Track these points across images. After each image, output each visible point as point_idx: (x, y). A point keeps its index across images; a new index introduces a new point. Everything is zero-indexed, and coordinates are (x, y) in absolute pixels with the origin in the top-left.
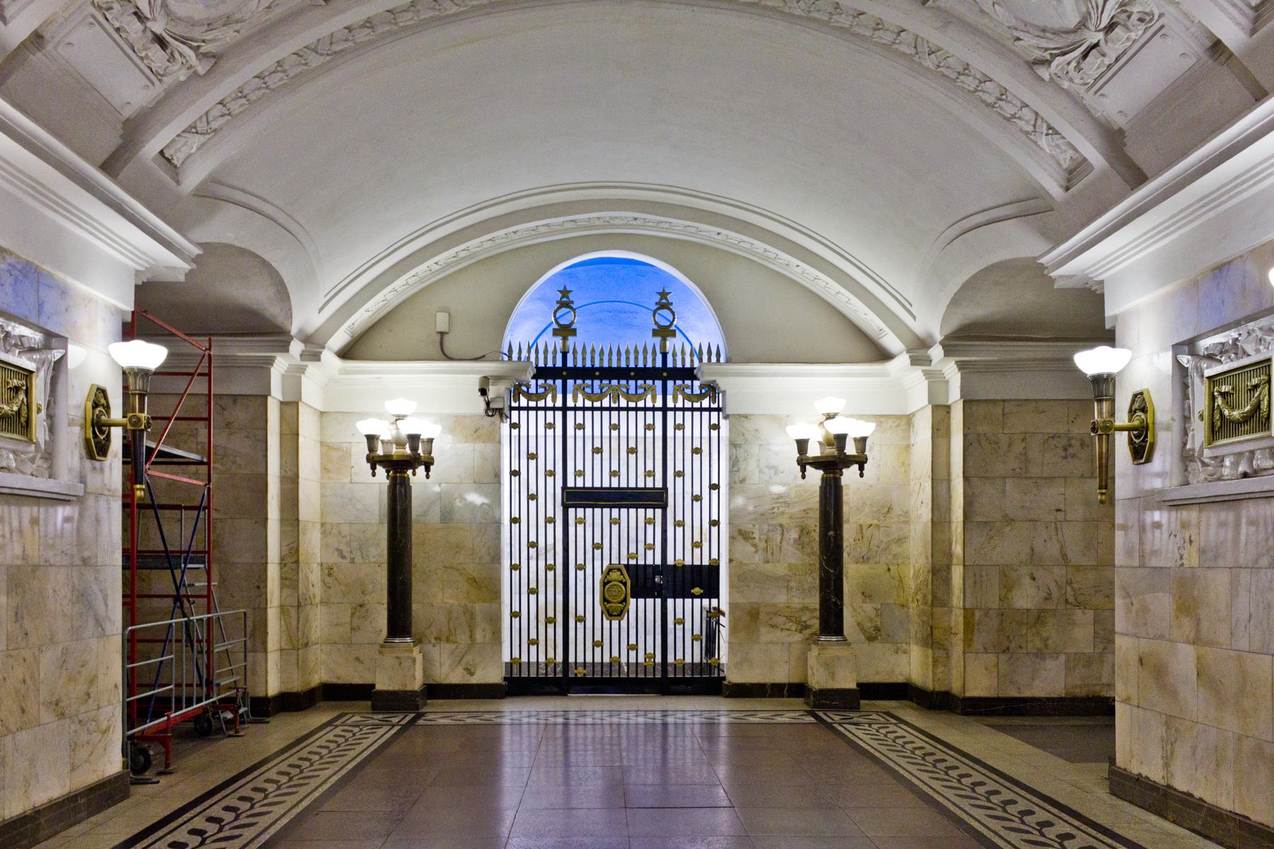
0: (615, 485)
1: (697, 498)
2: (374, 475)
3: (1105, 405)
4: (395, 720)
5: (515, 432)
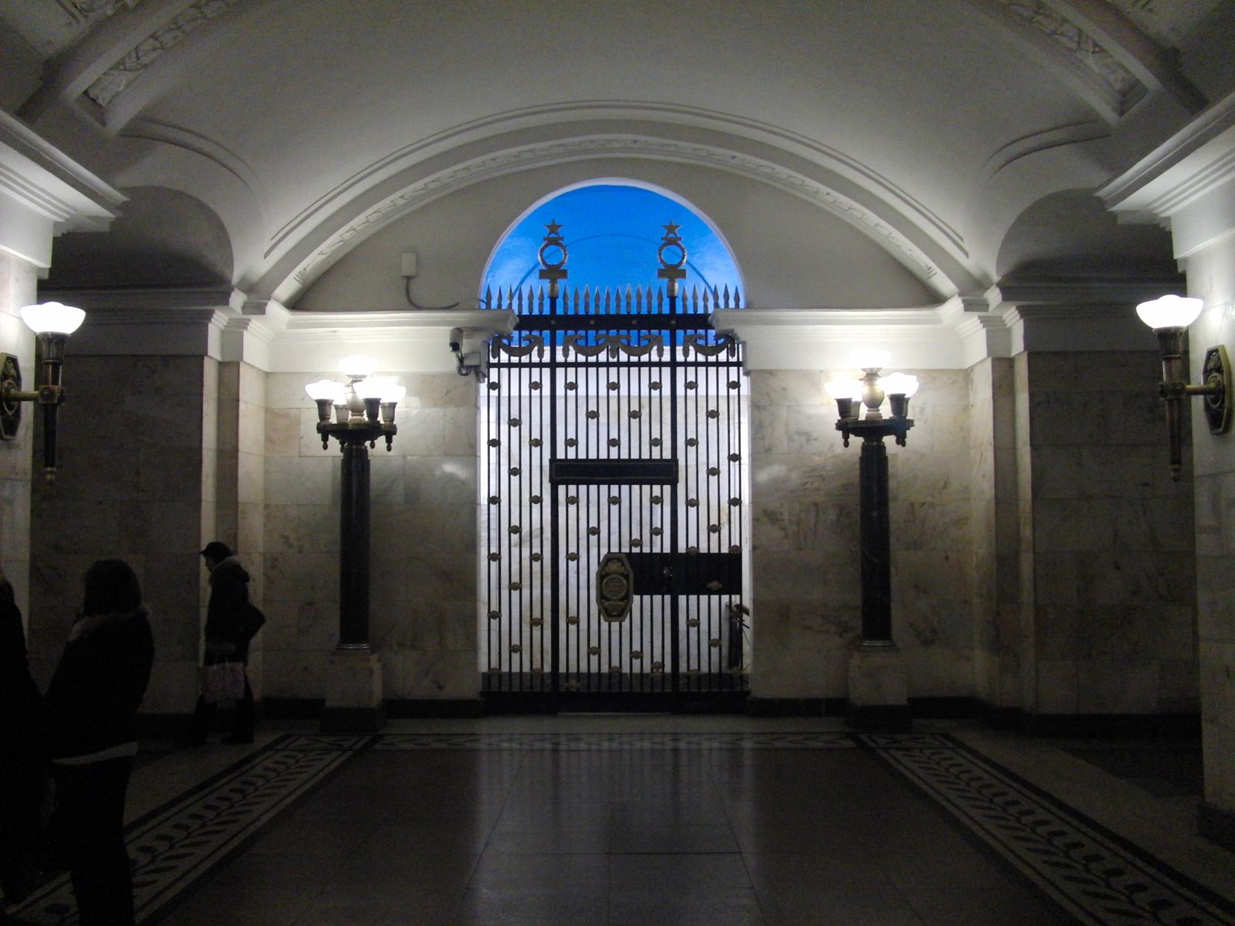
0: (614, 456)
1: (713, 472)
2: (325, 447)
3: (1176, 365)
4: (346, 744)
5: (494, 393)
